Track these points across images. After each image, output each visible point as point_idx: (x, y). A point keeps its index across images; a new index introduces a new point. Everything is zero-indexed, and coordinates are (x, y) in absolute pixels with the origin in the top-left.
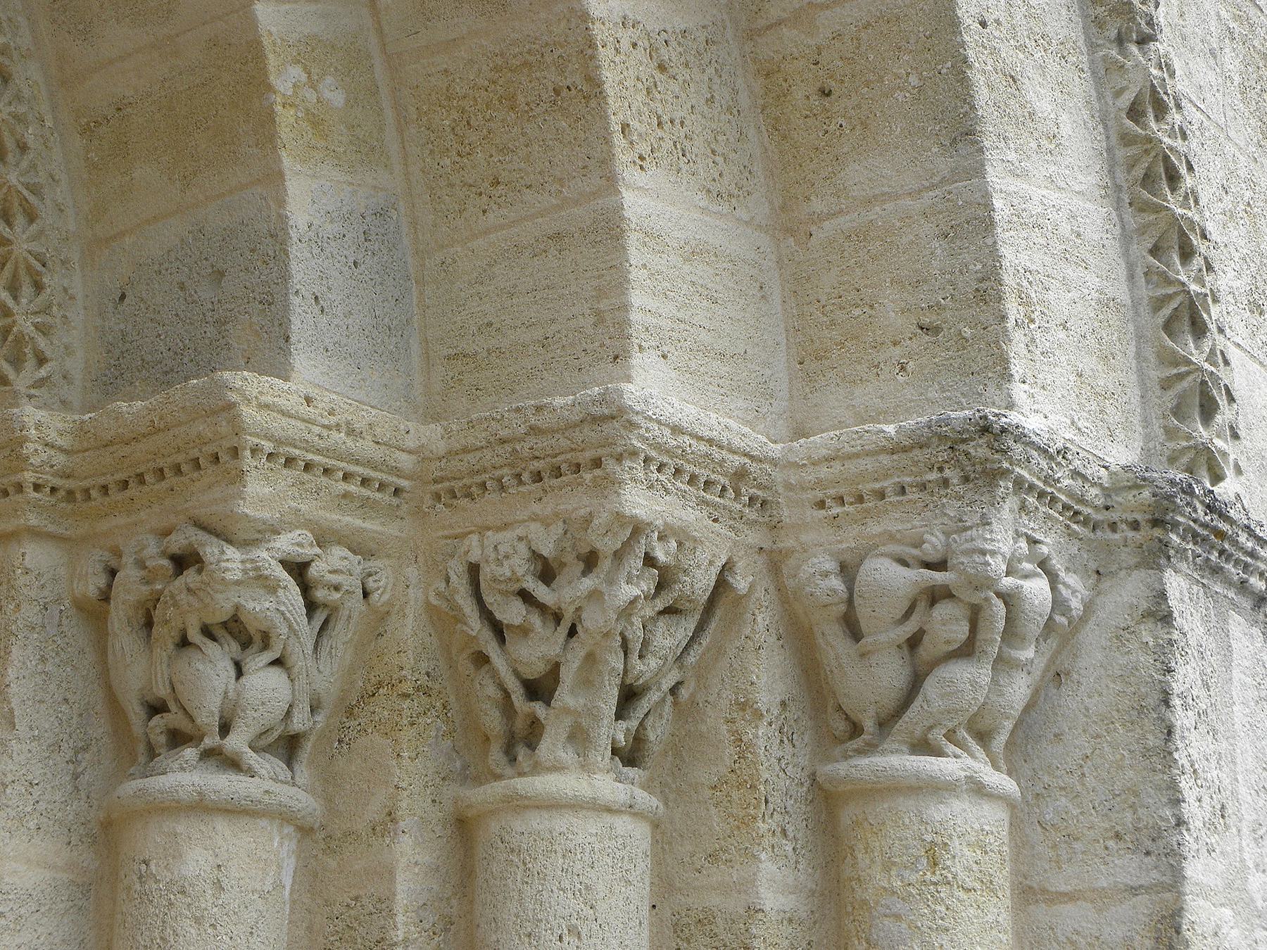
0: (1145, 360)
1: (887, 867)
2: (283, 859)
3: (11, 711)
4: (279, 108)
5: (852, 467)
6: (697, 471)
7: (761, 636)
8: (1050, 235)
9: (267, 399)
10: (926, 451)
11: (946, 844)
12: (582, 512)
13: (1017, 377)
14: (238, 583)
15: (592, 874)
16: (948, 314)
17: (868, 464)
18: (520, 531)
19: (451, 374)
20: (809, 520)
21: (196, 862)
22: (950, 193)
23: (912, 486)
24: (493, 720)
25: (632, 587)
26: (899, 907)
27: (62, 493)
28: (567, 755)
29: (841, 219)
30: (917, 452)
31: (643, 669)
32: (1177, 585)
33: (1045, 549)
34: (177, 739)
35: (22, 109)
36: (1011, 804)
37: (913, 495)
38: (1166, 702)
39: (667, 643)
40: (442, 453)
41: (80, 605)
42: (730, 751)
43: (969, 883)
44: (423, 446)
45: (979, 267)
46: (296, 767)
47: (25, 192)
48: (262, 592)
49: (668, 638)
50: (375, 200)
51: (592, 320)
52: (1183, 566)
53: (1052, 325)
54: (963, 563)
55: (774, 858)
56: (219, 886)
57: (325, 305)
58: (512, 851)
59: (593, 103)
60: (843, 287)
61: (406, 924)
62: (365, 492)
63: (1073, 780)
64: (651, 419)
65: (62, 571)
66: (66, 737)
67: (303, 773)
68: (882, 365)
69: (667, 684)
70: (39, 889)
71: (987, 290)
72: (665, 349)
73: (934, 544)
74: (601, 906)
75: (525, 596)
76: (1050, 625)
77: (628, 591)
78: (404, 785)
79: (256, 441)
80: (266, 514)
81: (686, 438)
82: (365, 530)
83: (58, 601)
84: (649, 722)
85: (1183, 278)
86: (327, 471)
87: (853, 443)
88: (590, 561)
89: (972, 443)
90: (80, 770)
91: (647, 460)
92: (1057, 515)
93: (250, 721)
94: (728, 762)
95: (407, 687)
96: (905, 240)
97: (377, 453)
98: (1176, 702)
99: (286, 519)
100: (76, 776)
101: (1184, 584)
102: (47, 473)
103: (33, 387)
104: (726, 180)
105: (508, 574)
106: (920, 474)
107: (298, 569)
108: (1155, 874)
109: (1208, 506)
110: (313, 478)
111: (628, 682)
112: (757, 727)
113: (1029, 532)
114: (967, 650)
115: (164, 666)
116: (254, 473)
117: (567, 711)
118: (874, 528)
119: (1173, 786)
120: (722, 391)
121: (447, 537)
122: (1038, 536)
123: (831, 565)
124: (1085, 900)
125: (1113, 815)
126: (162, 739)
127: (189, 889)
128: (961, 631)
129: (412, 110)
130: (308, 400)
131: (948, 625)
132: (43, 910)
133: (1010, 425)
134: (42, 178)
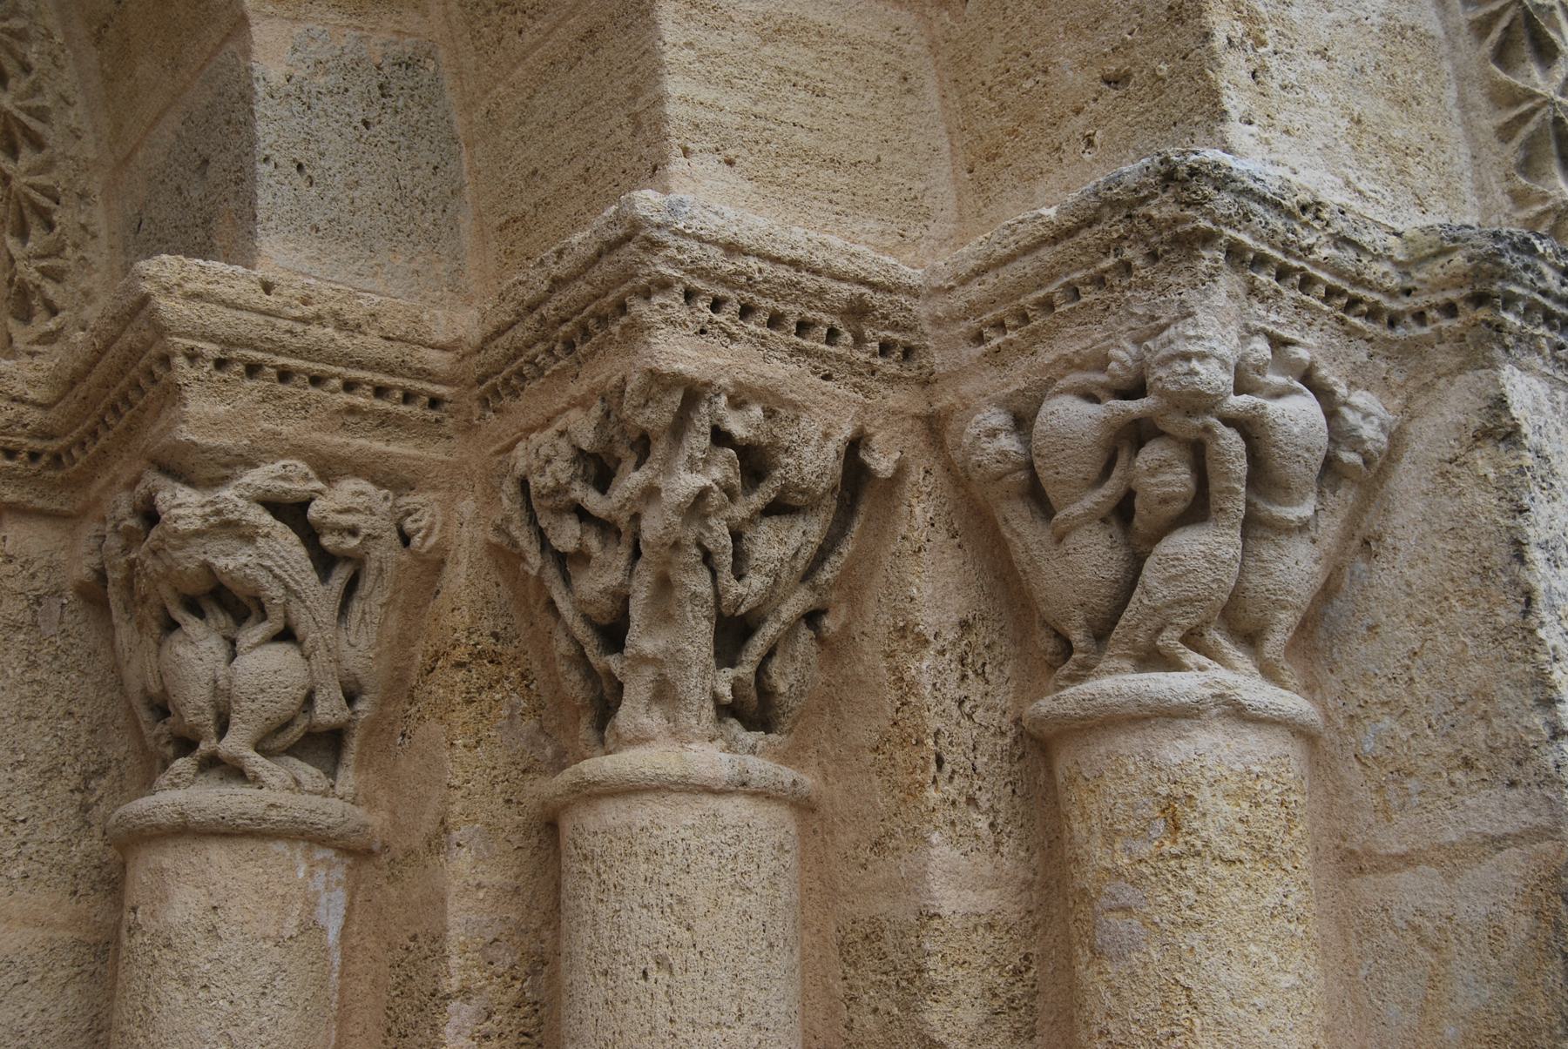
0: (1474, 107)
1: (1111, 835)
2: (317, 893)
5: (1008, 274)
6: (781, 308)
9: (198, 286)
10: (1096, 228)
11: (1191, 797)
12: (614, 380)
13: (1234, 114)
14: (198, 534)
15: (687, 881)
16: (1137, 53)
17: (1026, 266)
23: (1084, 284)
24: (574, 684)
26: (1128, 895)
27: (45, 458)
28: (653, 721)
30: (1085, 233)
32: (1524, 389)
33: (1303, 354)
34: (186, 744)
37: (1089, 296)
38: (1520, 557)
39: (776, 552)
42: (892, 694)
43: (1231, 853)
44: (459, 339)
47: (23, 117)
48: (236, 543)
49: (777, 545)
50: (398, 48)
51: (629, 130)
52: (1537, 361)
54: (1160, 379)
55: (953, 842)
57: (314, 175)
60: (1010, 57)
61: (464, 968)
62: (381, 405)
63: (1399, 690)
64: (684, 235)
66: (69, 759)
67: (348, 779)
68: (1064, 146)
70: (25, 953)
72: (731, 153)
73: (1124, 354)
74: (702, 926)
76: (1331, 469)
77: (687, 482)
78: (456, 783)
79: (189, 343)
80: (226, 441)
81: (752, 261)
82: (389, 456)
84: (775, 666)
86: (316, 381)
88: (643, 446)
89: (1154, 202)
92: (1318, 303)
93: (246, 715)
94: (890, 712)
95: (461, 654)
97: (392, 352)
98: (1536, 555)
99: (259, 445)
100: (85, 808)
101: (1541, 389)
102: (19, 435)
103: (38, 342)
105: (551, 484)
106: (1093, 264)
107: (291, 511)
108: (1525, 815)
110: (294, 390)
113: (1270, 328)
114: (1198, 510)
115: (153, 655)
116: (196, 386)
117: (643, 660)
118: (1047, 356)
119: (1541, 680)
120: (837, 208)
122: (1286, 334)
123: (997, 418)
124: (1429, 863)
126: (170, 751)
127: (176, 941)
128: (1178, 480)
130: (267, 287)
131: (1162, 474)
133: (1202, 163)
134: (47, 101)
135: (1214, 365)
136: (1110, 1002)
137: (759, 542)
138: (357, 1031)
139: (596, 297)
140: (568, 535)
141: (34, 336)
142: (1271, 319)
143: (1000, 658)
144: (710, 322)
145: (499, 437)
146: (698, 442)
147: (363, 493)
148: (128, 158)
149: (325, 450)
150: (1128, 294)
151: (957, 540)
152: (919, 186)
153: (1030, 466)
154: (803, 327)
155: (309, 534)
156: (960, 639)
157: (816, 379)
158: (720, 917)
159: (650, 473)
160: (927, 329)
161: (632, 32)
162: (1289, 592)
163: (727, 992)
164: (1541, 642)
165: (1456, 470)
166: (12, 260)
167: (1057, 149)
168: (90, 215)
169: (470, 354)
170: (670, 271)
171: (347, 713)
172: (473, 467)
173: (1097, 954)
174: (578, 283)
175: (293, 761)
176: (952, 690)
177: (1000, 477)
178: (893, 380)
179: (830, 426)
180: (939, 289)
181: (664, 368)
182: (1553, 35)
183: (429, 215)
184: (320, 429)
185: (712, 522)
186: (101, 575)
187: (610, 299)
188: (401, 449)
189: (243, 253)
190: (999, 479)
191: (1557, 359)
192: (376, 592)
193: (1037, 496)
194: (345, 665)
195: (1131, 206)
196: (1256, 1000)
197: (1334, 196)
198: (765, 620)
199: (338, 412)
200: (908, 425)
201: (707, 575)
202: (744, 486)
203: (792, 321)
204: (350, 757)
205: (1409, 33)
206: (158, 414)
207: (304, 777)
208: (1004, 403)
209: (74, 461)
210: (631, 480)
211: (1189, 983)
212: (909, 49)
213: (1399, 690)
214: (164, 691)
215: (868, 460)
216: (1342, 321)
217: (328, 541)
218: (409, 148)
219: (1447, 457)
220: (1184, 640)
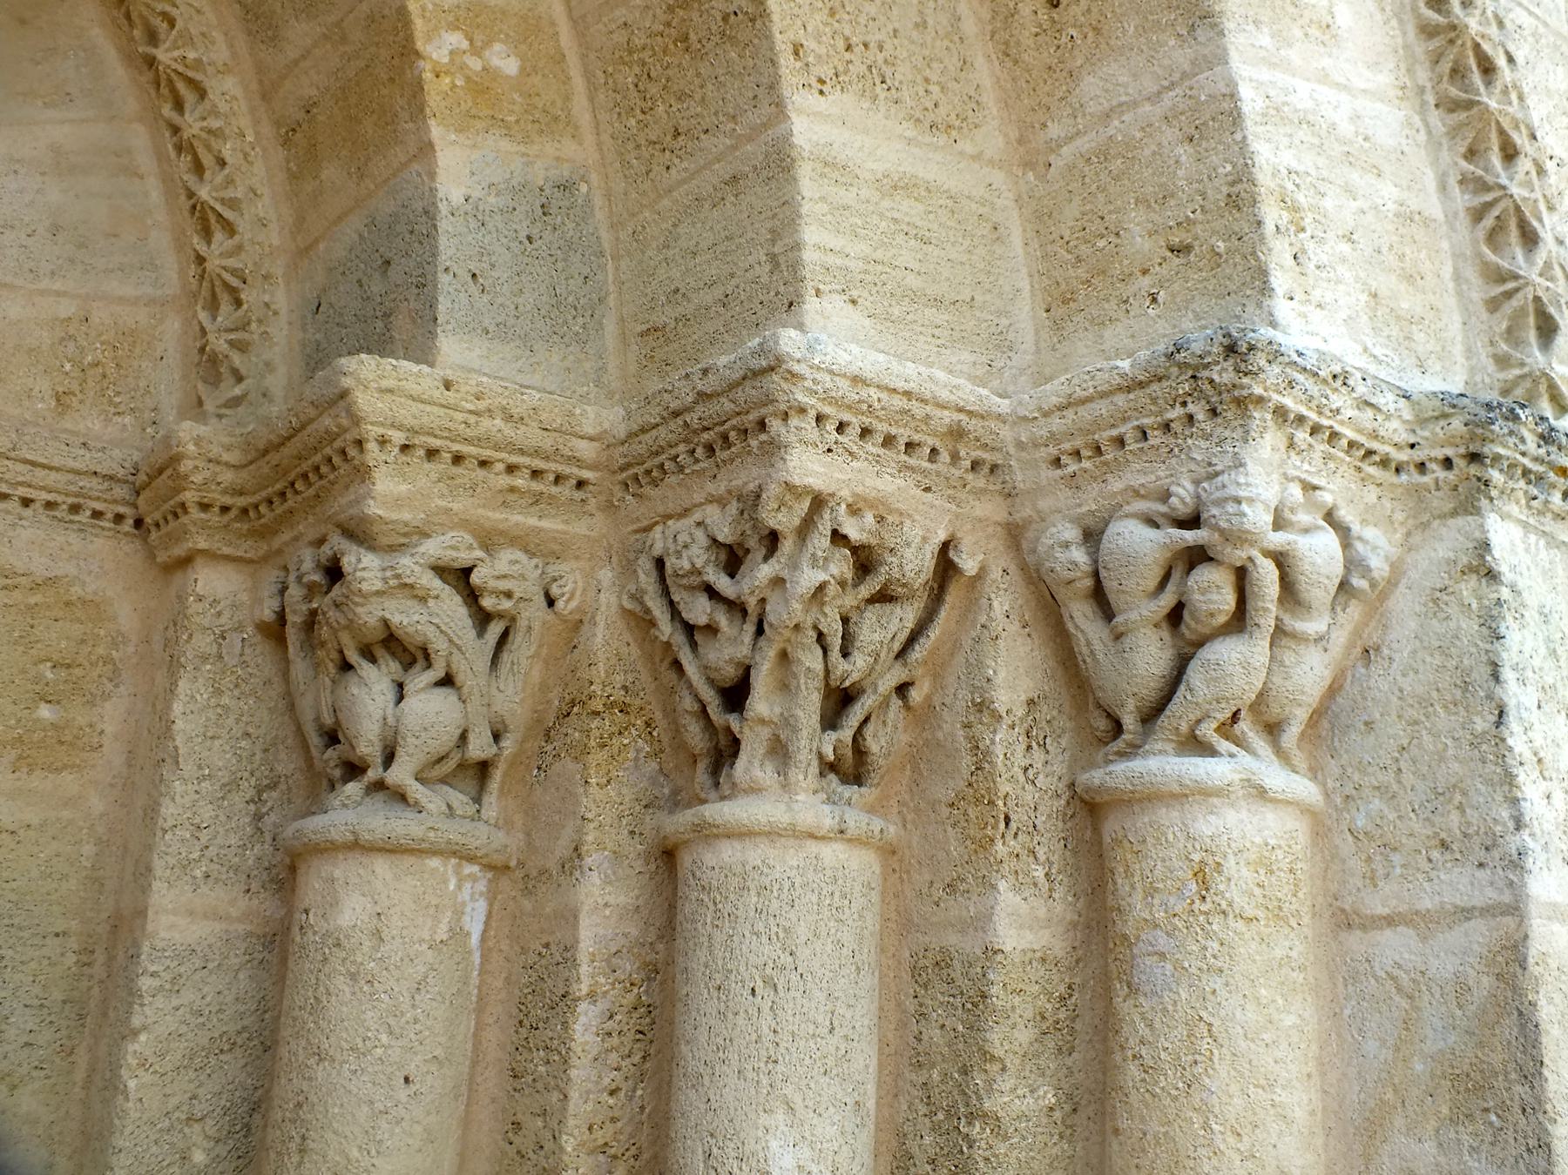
2: (464, 904)
3: (176, 748)
4: (428, 76)
6: (893, 431)
8: (1323, 133)
10: (1165, 384)
11: (1219, 864)
12: (751, 486)
13: (1280, 291)
14: (378, 593)
16: (1199, 229)
17: (1102, 408)
18: (697, 516)
20: (1044, 482)
21: (352, 912)
22: (1191, 89)
24: (695, 735)
25: (818, 568)
26: (1163, 942)
27: (233, 513)
29: (1078, 142)
30: (1155, 386)
31: (853, 669)
34: (354, 769)
35: (215, 124)
36: (1306, 810)
38: (1496, 677)
39: (876, 637)
40: (623, 436)
41: (262, 628)
42: (966, 762)
43: (1249, 913)
44: (606, 431)
45: (1229, 168)
46: (486, 799)
47: (218, 207)
49: (880, 630)
51: (768, 268)
52: (1514, 509)
53: (1330, 235)
55: (1016, 889)
56: (378, 935)
58: (704, 888)
59: (758, 24)
62: (536, 486)
64: (819, 368)
65: (244, 597)
66: (246, 775)
67: (492, 805)
69: (888, 682)
71: (1240, 196)
72: (855, 293)
73: (1183, 495)
74: (803, 953)
77: (809, 578)
78: (589, 815)
80: (406, 516)
82: (541, 530)
83: (239, 628)
85: (1504, 181)
86: (483, 464)
90: (264, 810)
92: (1342, 455)
96: (1147, 152)
97: (547, 442)
98: (1508, 674)
99: (436, 520)
100: (258, 817)
101: (1516, 532)
104: (942, 110)
107: (460, 577)
109: (1542, 437)
111: (833, 684)
112: (995, 731)
113: (1303, 476)
114: (1240, 620)
115: (328, 691)
116: (384, 468)
117: (762, 721)
118: (1116, 485)
121: (636, 531)
122: (1315, 481)
123: (1071, 533)
125: (1437, 819)
126: (337, 773)
127: (345, 942)
128: (1226, 600)
129: (600, 74)
130: (448, 385)
131: (1212, 592)
132: (211, 966)
134: (239, 192)
135: (1261, 507)
136: (1143, 1030)
138: (491, 1021)
140: (699, 610)
141: (221, 401)
142: (1301, 467)
143: (1058, 731)
145: (638, 519)
146: (820, 541)
148: (308, 249)
149: (487, 525)
150: (1190, 441)
152: (1004, 322)
153: (1096, 574)
154: (910, 446)
155: (471, 596)
157: (919, 492)
158: (818, 946)
160: (1012, 450)
161: (773, 184)
162: (1303, 693)
163: (822, 1009)
164: (1510, 749)
165: (1446, 598)
166: (203, 331)
167: (1126, 302)
168: (272, 295)
169: (614, 445)
171: (494, 749)
173: (1133, 990)
174: (723, 400)
175: (446, 788)
176: (1020, 759)
178: (979, 493)
180: (1025, 419)
181: (797, 481)
182: (1535, 224)
183: (580, 320)
185: (827, 609)
186: (281, 617)
187: (751, 417)
189: (423, 353)
191: (1529, 507)
193: (1099, 595)
195: (1196, 368)
196: (1265, 1036)
197: (1354, 359)
198: (864, 691)
201: (819, 652)
203: (902, 442)
204: (494, 784)
205: (1417, 217)
206: (347, 487)
207: (455, 805)
208: (1076, 520)
209: (260, 516)
211: (1210, 1019)
212: (999, 203)
213: (1390, 777)
214: (337, 722)
215: (956, 559)
216: (1359, 469)
217: (487, 602)
218: (565, 260)
219: (1438, 586)
220: (1217, 730)
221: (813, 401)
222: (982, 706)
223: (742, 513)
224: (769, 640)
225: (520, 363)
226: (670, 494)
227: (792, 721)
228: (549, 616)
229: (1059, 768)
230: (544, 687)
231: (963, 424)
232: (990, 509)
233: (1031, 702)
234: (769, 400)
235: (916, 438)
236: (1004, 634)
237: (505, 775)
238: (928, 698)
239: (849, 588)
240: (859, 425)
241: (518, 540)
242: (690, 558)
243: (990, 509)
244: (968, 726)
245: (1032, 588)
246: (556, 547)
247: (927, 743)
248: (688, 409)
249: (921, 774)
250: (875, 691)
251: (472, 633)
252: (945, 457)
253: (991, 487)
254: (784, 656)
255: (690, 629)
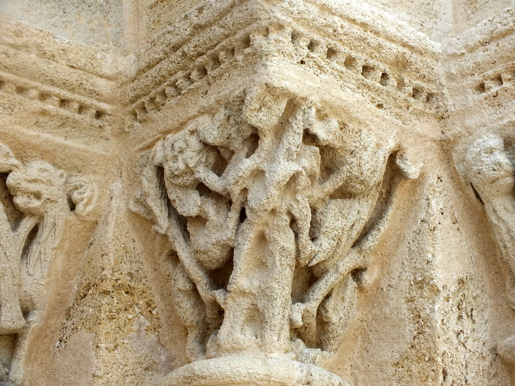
6: (354, 54)
7: (436, 218)
12: (237, 93)
18: (191, 126)
19: (152, 19)
20: (471, 104)
25: (290, 161)
28: (245, 336)
31: (319, 250)
39: (339, 224)
42: (410, 329)
44: (120, 73)
46: (15, 364)
49: (343, 219)
69: (347, 264)
75: (202, 188)
77: (285, 168)
78: (99, 373)
81: (336, 19)
82: (66, 147)
84: (331, 304)
86: (21, 90)
87: (505, 21)
91: (295, 36)
95: (107, 286)
97: (74, 77)
111: (303, 262)
112: (434, 302)
117: (243, 293)
121: (142, 149)
137: (329, 216)
139: (227, 36)
140: (191, 204)
143: (482, 306)
144: (308, 56)
145: (144, 139)
146: (294, 138)
147: (46, 170)
149: (23, 139)
151: (457, 225)
154: (366, 69)
156: (458, 291)
157: (373, 107)
159: (258, 160)
160: (444, 82)
169: (126, 83)
170: (284, 18)
171: (23, 322)
172: (122, 160)
177: (494, 181)
179: (381, 139)
180: (454, 56)
181: (276, 83)
184: (20, 124)
185: (299, 197)
188: (74, 144)
190: (493, 182)
192: (50, 238)
194: (24, 288)
198: (327, 271)
199: (34, 113)
200: (428, 144)
201: (292, 235)
202: (321, 175)
203: (360, 63)
204: (22, 352)
208: (498, 131)
210: (244, 165)
215: (402, 166)
221: (290, 20)
222: (423, 283)
223: (228, 118)
224: (251, 224)
225: (54, 20)
226: (169, 113)
227: (268, 292)
228: (72, 217)
229: (483, 335)
230: (66, 275)
231: (407, 56)
232: (428, 128)
233: (461, 282)
234: (254, 19)
235: (371, 62)
236: (440, 227)
237: (32, 345)
238: (377, 282)
239: (316, 184)
240: (324, 49)
241: (46, 154)
242: (184, 160)
243: (428, 128)
244: (411, 300)
245: (461, 193)
246: (78, 162)
247: (375, 318)
248: (186, 42)
249: (370, 343)
250: (337, 271)
251: (7, 226)
252: (393, 81)
253: (428, 111)
254: (262, 239)
255: (183, 222)
